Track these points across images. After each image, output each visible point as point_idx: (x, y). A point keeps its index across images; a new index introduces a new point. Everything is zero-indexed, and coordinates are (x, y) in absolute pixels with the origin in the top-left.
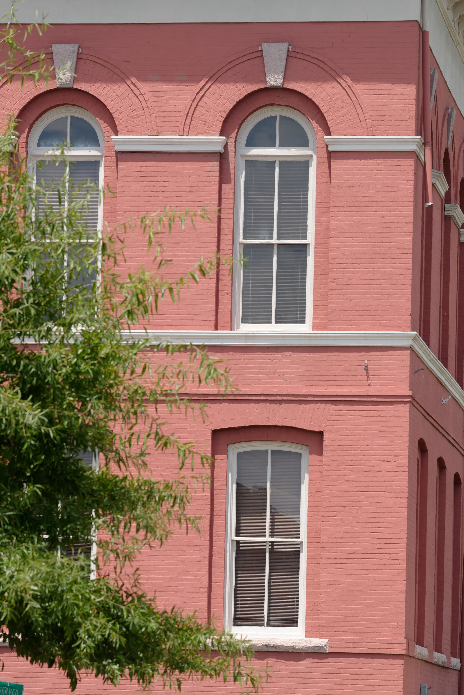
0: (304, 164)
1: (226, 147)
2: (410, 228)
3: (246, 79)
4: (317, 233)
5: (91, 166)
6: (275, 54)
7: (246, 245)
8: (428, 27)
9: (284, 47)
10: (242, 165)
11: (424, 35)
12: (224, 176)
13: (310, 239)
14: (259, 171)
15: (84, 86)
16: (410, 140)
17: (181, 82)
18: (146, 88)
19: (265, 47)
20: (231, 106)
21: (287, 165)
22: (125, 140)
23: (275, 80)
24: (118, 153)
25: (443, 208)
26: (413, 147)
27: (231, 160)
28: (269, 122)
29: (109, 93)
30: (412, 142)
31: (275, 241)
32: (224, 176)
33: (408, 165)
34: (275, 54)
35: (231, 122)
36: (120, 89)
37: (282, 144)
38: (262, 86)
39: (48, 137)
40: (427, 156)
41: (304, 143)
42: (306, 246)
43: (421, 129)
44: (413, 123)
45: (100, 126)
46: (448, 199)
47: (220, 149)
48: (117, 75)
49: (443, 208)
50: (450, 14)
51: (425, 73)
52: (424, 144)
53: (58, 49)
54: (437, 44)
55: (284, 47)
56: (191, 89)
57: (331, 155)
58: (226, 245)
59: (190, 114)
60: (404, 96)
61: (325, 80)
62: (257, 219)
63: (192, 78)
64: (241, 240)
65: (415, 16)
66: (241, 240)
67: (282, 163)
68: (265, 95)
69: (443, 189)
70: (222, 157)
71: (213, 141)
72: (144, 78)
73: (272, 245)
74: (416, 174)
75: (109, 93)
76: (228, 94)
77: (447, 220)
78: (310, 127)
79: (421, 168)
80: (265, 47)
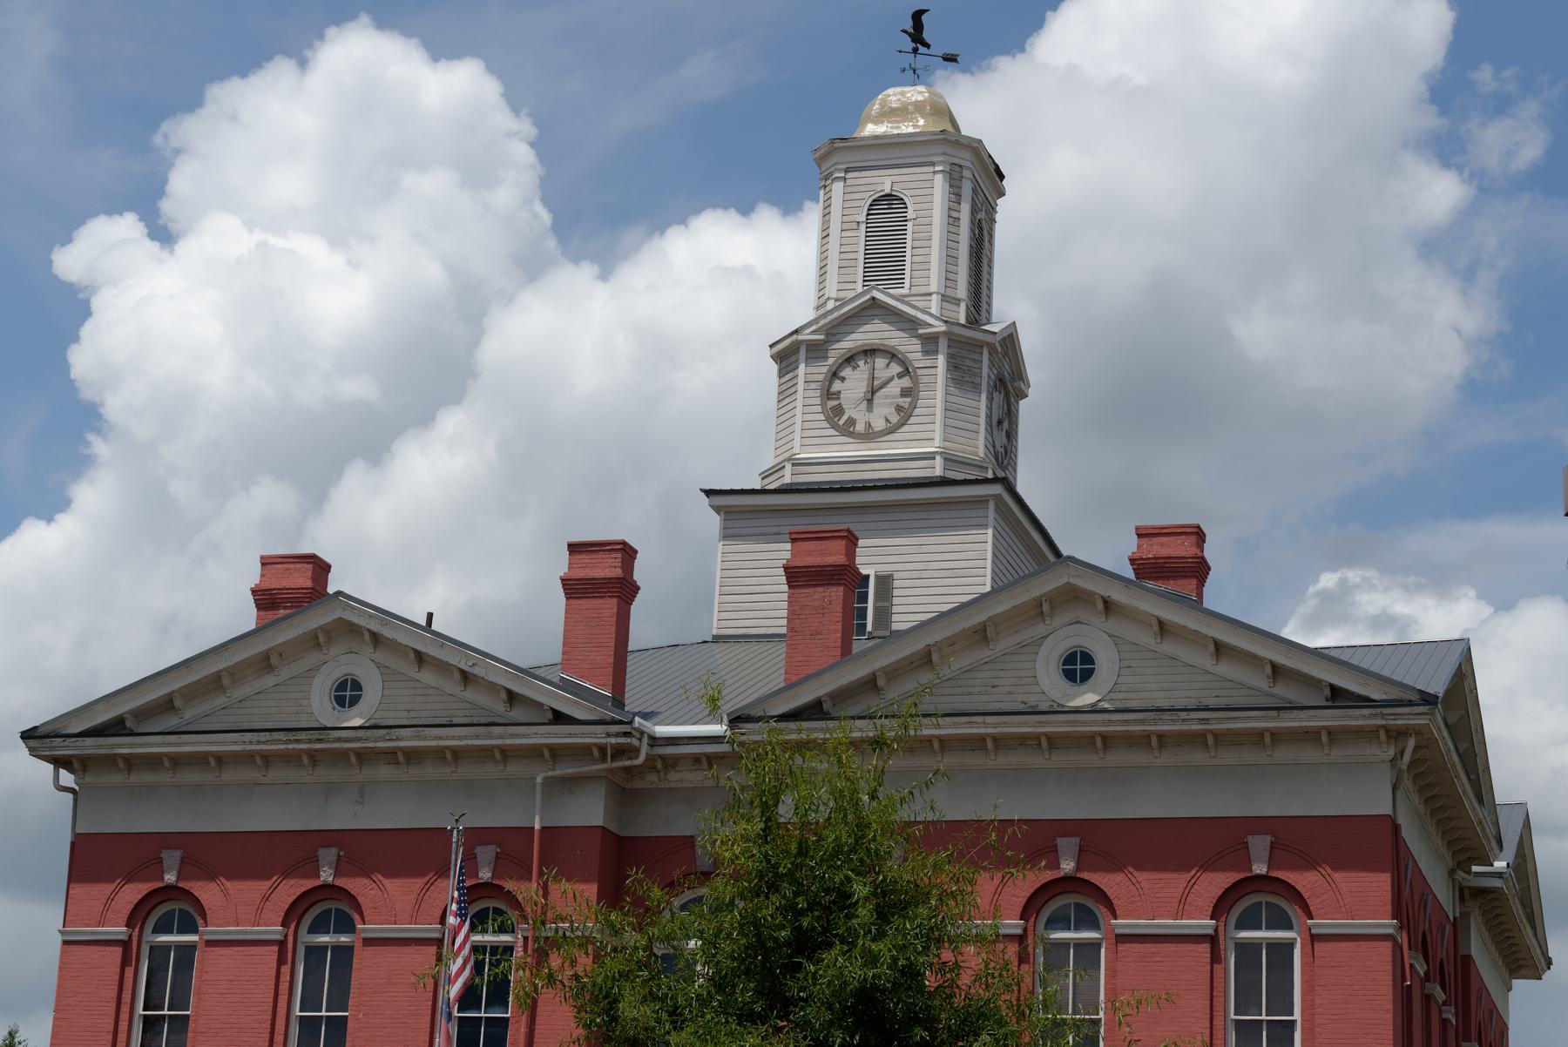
0: (1289, 946)
1: (1216, 930)
2: (1390, 1006)
3: (1233, 868)
4: (1303, 1010)
5: (1095, 946)
6: (1259, 845)
7: (1237, 1021)
8: (1401, 820)
9: (1268, 838)
10: (1231, 946)
11: (1396, 828)
12: (1216, 957)
13: (1297, 1016)
14: (1248, 952)
15: (1085, 875)
16: (1387, 925)
17: (1174, 871)
18: (1142, 877)
19: (1250, 838)
20: (1220, 893)
21: (1273, 946)
22: (1123, 924)
23: (1260, 868)
24: (1117, 936)
25: (1423, 987)
26: (1390, 931)
27: (1222, 942)
28: (170, 914)
29: (1106, 881)
30: (1390, 926)
31: (1264, 1017)
32: (1216, 957)
33: (1387, 947)
34: (1259, 845)
35: (1219, 909)
36: (1120, 877)
37: (1269, 928)
38: (161, 885)
39: (1052, 923)
40: (1403, 939)
41: (1289, 927)
42: (1294, 1022)
43: (1396, 915)
44: (1389, 907)
45: (1100, 911)
46: (1427, 977)
47: (1211, 931)
48: (1115, 865)
49: (1423, 987)
50: (1422, 808)
51: (1398, 862)
52: (1401, 928)
53: (1062, 842)
54: (1410, 834)
55: (1268, 838)
56: (420, 882)
57: (1314, 938)
58: (1218, 1022)
59: (1183, 900)
60: (1379, 884)
61: (1306, 869)
62: (1246, 999)
63: (1183, 867)
64: (1232, 1016)
65: (1388, 810)
66: (1232, 1016)
67: (1268, 945)
68: (1253, 883)
69: (1421, 970)
70: (1213, 940)
71: (1205, 924)
72: (1140, 868)
73: (1261, 1021)
74: (1394, 956)
75: (1106, 881)
76: (134, 892)
77: (1428, 999)
78: (1294, 912)
79: (1397, 948)
80: (1250, 838)
